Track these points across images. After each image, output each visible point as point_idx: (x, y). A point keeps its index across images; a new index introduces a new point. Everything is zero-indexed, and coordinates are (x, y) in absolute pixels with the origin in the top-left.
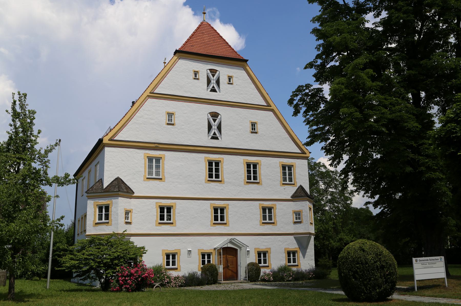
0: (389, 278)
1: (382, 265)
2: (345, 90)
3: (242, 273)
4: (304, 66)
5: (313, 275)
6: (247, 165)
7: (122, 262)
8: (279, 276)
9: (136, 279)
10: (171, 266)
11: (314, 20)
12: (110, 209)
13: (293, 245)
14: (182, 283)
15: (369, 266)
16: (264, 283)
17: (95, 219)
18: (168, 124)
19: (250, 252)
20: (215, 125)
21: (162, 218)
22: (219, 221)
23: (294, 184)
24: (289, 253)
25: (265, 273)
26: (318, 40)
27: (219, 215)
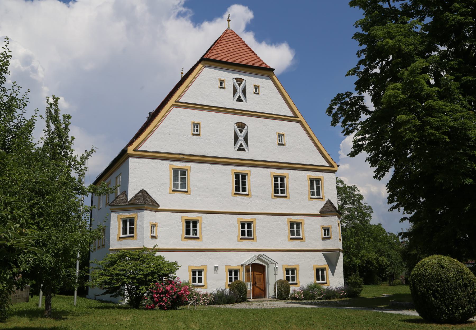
0: (473, 298)
1: (465, 284)
2: (402, 96)
3: (271, 291)
4: (346, 74)
5: (344, 293)
6: (236, 175)
7: (155, 278)
8: (309, 295)
9: (171, 296)
10: (197, 283)
11: (356, 25)
12: (135, 223)
13: (323, 263)
14: (210, 301)
15: (451, 285)
16: (295, 301)
17: (119, 232)
18: (194, 134)
19: (278, 269)
20: (241, 136)
21: (188, 232)
22: (246, 236)
23: (322, 199)
24: (317, 270)
25: (295, 291)
26: (361, 45)
27: (246, 230)
